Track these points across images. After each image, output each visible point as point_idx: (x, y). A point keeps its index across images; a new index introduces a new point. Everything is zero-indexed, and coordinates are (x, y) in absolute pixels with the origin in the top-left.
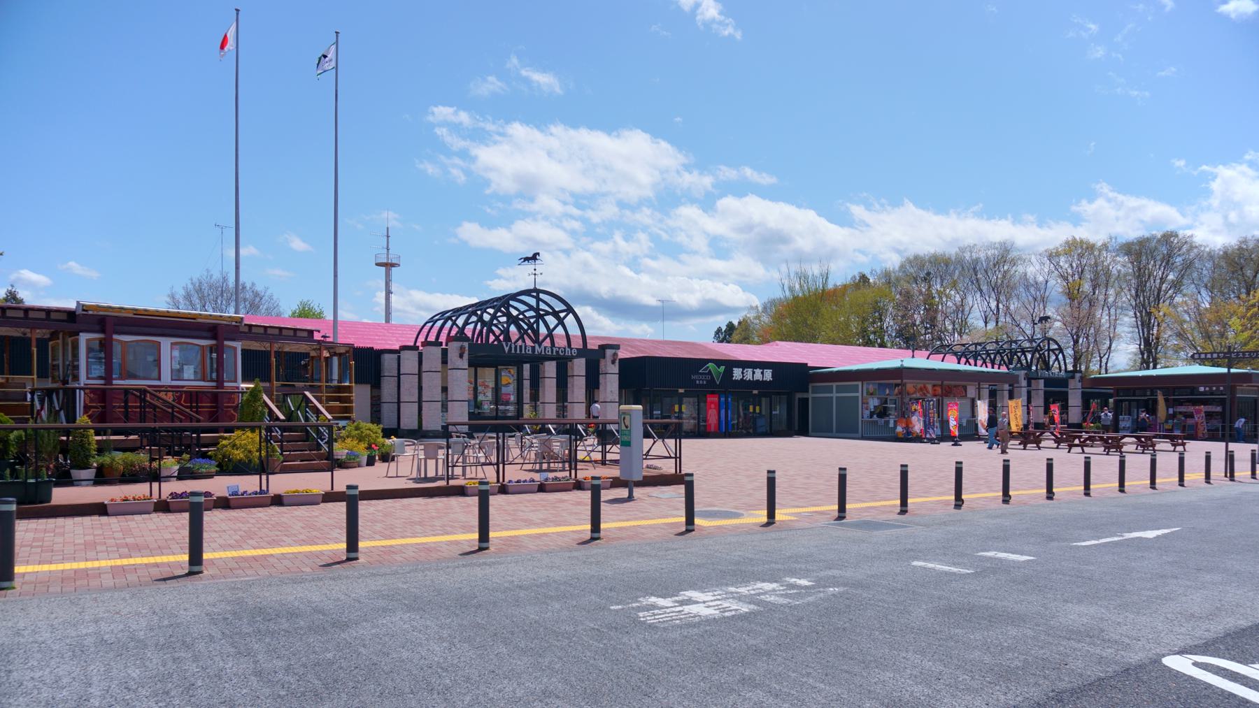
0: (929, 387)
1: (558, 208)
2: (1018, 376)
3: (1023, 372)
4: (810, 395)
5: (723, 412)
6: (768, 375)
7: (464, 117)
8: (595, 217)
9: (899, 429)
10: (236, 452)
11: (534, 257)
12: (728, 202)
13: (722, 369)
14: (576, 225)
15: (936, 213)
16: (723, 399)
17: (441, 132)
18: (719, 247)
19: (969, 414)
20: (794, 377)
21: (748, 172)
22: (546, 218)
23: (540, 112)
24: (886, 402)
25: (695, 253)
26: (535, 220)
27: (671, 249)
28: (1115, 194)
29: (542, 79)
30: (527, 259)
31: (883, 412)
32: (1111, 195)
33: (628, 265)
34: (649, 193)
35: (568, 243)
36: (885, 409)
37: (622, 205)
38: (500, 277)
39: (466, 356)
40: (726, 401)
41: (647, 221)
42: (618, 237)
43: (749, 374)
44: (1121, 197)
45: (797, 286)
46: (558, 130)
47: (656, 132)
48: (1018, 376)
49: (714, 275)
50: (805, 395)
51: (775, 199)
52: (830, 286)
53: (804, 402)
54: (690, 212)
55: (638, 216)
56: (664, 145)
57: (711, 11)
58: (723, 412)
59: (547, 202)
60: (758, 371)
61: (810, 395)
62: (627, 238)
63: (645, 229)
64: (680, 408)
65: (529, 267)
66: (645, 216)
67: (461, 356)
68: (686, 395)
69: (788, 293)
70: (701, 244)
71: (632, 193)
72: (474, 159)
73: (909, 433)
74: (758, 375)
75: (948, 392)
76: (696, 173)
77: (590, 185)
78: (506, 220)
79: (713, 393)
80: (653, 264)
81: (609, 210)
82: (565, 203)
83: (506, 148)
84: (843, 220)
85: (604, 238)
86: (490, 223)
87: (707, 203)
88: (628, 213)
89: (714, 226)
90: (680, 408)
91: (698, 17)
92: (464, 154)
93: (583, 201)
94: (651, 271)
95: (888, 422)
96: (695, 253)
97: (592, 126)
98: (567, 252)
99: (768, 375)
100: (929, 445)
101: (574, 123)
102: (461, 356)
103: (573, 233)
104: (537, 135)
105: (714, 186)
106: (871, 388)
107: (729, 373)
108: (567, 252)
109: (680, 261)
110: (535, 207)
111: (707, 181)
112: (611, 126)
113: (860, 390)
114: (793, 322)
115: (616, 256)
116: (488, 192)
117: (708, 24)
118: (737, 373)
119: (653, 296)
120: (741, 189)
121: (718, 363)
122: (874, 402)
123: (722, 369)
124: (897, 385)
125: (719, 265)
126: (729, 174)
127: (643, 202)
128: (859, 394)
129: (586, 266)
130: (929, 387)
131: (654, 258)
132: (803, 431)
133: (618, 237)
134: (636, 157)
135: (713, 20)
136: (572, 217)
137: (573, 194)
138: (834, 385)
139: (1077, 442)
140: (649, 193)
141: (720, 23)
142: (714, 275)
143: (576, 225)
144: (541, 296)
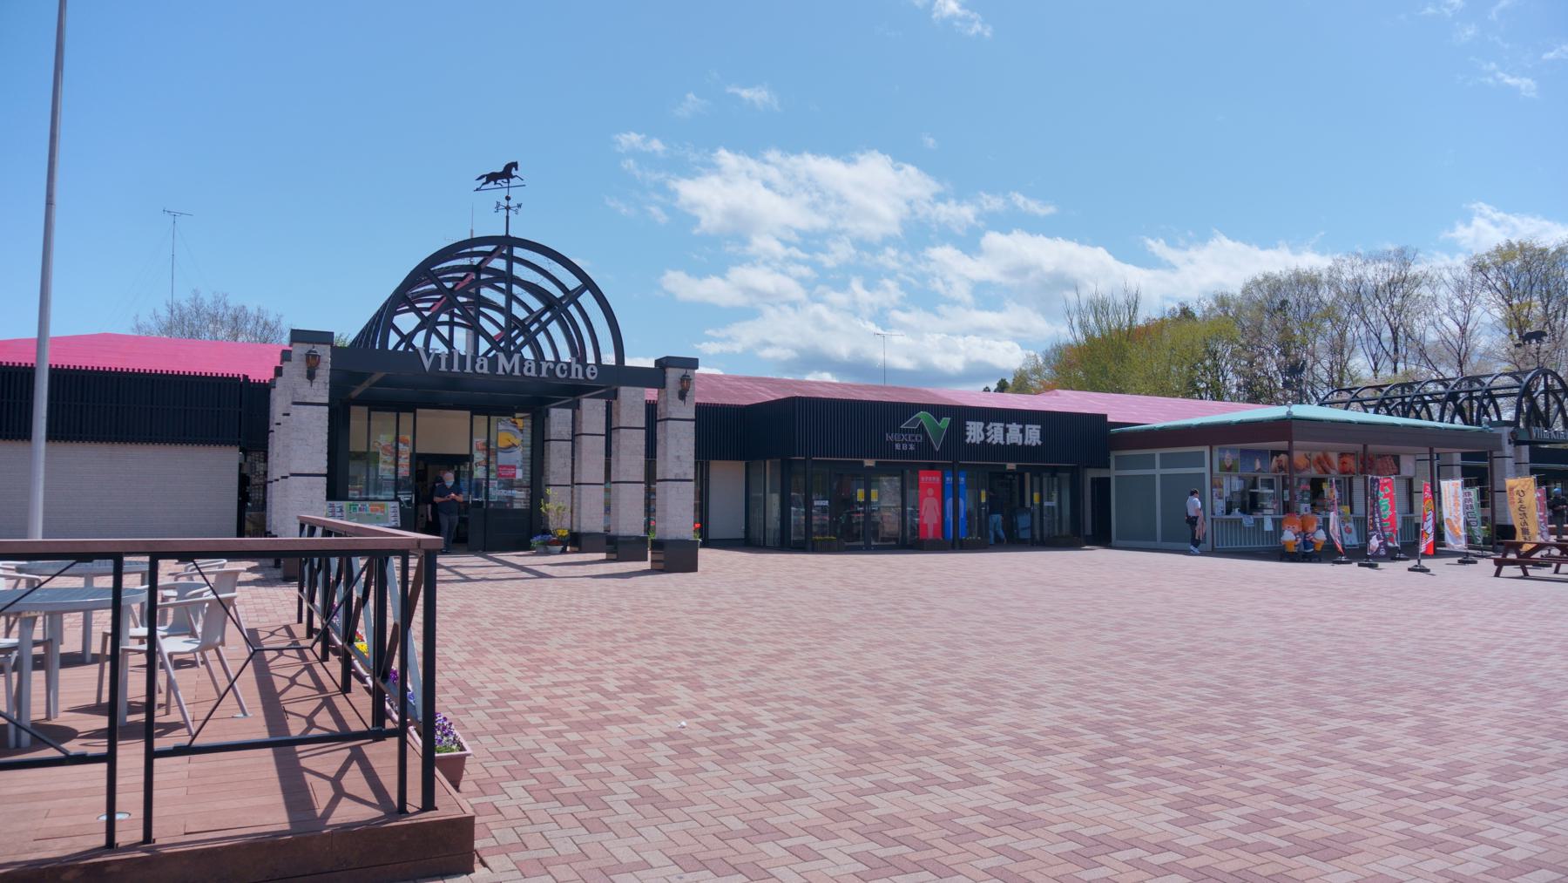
0: (1334, 457)
1: (777, 248)
2: (1500, 436)
3: (1506, 430)
4: (1113, 473)
5: (949, 503)
6: (1033, 435)
7: (657, 145)
8: (828, 261)
9: (1289, 536)
10: (1477, 533)
11: (507, 173)
12: (994, 239)
13: (945, 422)
14: (805, 271)
15: (1263, 248)
16: (949, 479)
17: (629, 164)
18: (987, 296)
19: (1405, 507)
20: (1081, 442)
21: (1019, 199)
22: (766, 263)
23: (754, 137)
24: (1255, 486)
25: (954, 303)
26: (754, 265)
27: (924, 297)
28: (1501, 215)
29: (756, 95)
30: (492, 177)
31: (1251, 503)
32: (1497, 216)
33: (872, 319)
34: (896, 230)
35: (798, 293)
36: (1254, 497)
37: (862, 244)
38: (710, 339)
39: (324, 373)
40: (956, 483)
41: (893, 265)
42: (856, 286)
43: (996, 434)
44: (1513, 220)
45: (1092, 320)
46: (773, 155)
47: (901, 153)
48: (1500, 436)
49: (982, 331)
50: (1102, 473)
51: (1050, 234)
52: (1140, 321)
53: (1102, 486)
54: (944, 254)
55: (881, 259)
56: (911, 169)
57: (952, 7)
58: (949, 503)
59: (764, 243)
60: (1014, 428)
61: (1113, 473)
62: (868, 287)
63: (891, 275)
64: (868, 496)
65: (496, 193)
66: (890, 258)
67: (311, 376)
68: (883, 469)
69: (1078, 334)
70: (961, 291)
71: (872, 230)
72: (674, 194)
73: (1307, 543)
74: (1014, 435)
75: (1367, 464)
76: (952, 202)
77: (822, 222)
78: (720, 268)
79: (932, 467)
80: (902, 317)
81: (842, 252)
82: (787, 244)
83: (715, 180)
84: (1149, 261)
85: (842, 286)
86: (700, 272)
87: (969, 243)
88: (867, 255)
89: (980, 269)
90: (868, 496)
91: (935, 15)
92: (661, 187)
93: (811, 242)
94: (903, 327)
95: (1260, 522)
96: (954, 303)
97: (819, 150)
98: (794, 305)
99: (1033, 435)
100: (1351, 572)
101: (793, 146)
102: (311, 376)
103: (801, 280)
104: (752, 164)
105: (978, 217)
106: (1229, 458)
107: (958, 429)
108: (794, 305)
109: (937, 314)
110: (752, 250)
111: (967, 212)
112: (844, 150)
113: (1209, 460)
114: (1086, 372)
115: (854, 310)
116: (696, 231)
117: (949, 21)
118: (974, 432)
119: (909, 357)
120: (1006, 222)
121: (938, 410)
122: (1233, 484)
123: (945, 422)
124: (1276, 453)
125: (989, 318)
126: (996, 204)
127: (888, 241)
128: (1206, 470)
129: (819, 322)
130: (1334, 457)
131: (904, 310)
132: (1101, 537)
133: (856, 286)
134: (876, 187)
135: (953, 17)
136: (797, 261)
137: (799, 232)
138: (1158, 452)
139: (1512, 556)
140: (896, 230)
141: (964, 20)
142: (982, 331)
143: (805, 271)
144: (518, 252)
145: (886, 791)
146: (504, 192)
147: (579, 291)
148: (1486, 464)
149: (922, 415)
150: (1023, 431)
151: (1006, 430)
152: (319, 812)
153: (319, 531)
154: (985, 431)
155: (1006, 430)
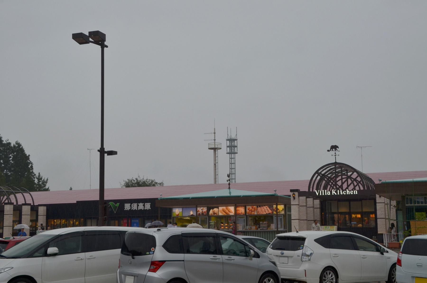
6: (148, 206)
13: (118, 205)
43: (135, 207)
65: (332, 152)
74: (141, 206)
99: (148, 206)
118: (127, 207)
121: (115, 201)
123: (118, 205)
145: (140, 254)
146: (334, 152)
147: (342, 177)
148: (42, 211)
149: (111, 203)
150: (144, 205)
151: (138, 205)
152: (3, 254)
153: (18, 227)
154: (131, 206)
155: (138, 205)
